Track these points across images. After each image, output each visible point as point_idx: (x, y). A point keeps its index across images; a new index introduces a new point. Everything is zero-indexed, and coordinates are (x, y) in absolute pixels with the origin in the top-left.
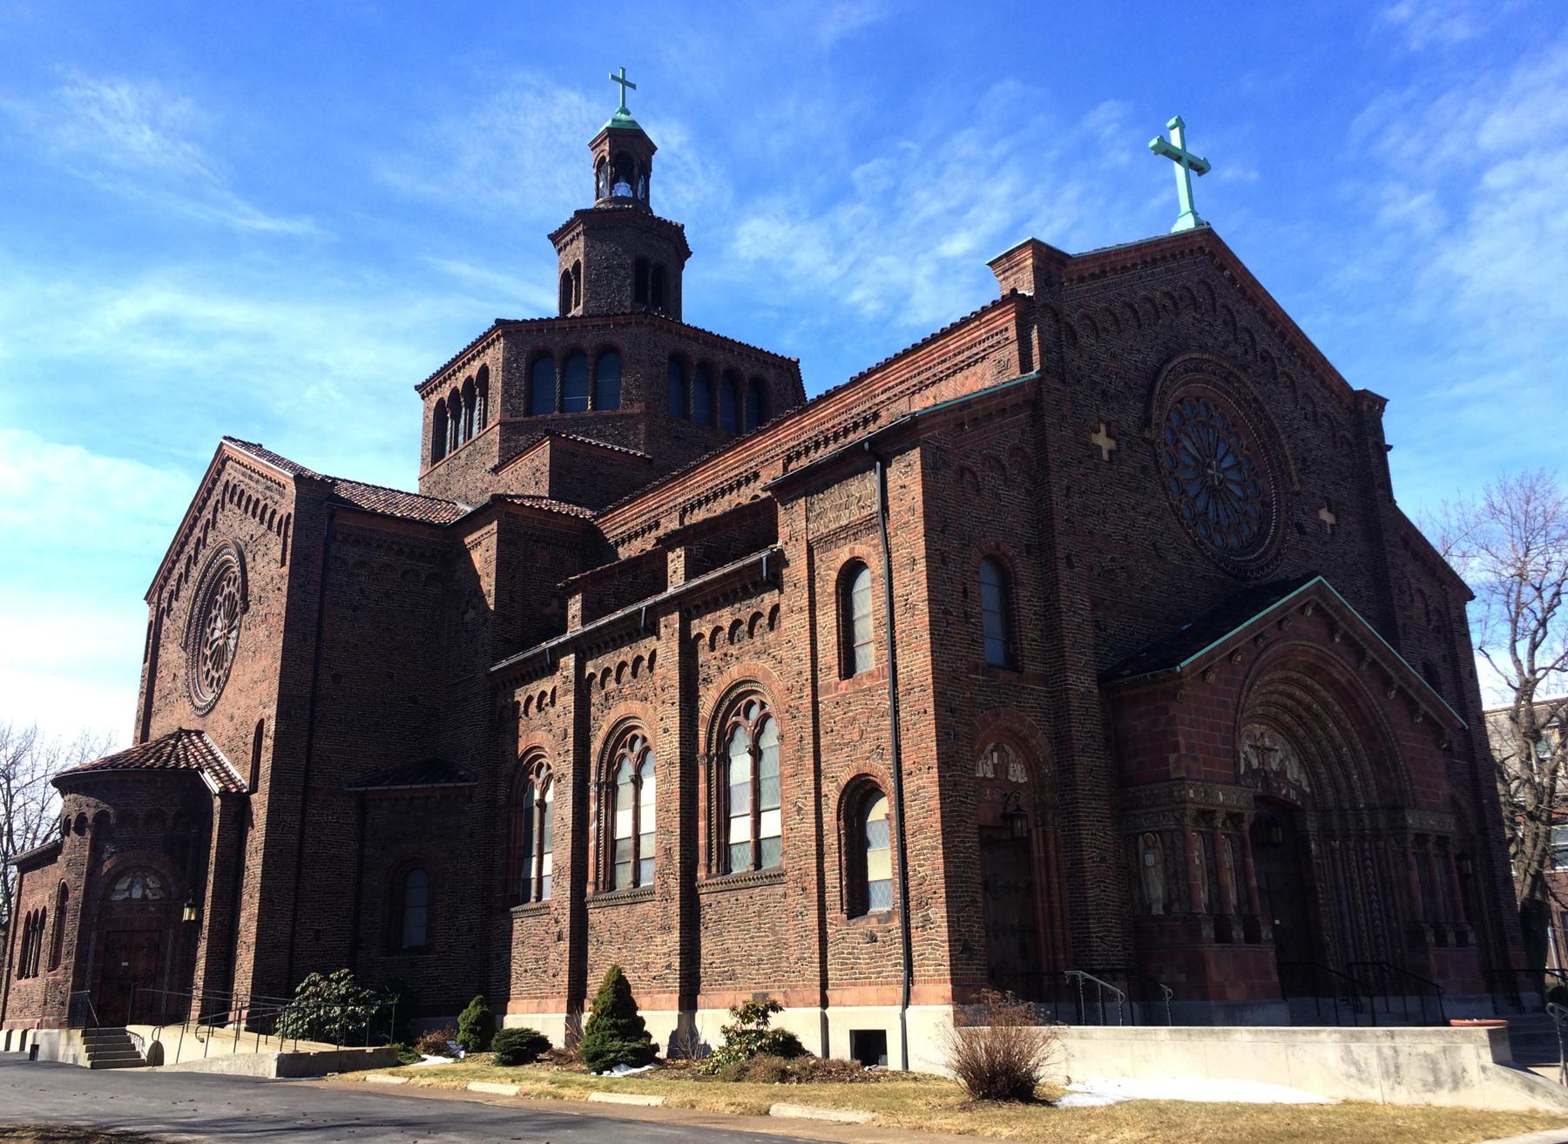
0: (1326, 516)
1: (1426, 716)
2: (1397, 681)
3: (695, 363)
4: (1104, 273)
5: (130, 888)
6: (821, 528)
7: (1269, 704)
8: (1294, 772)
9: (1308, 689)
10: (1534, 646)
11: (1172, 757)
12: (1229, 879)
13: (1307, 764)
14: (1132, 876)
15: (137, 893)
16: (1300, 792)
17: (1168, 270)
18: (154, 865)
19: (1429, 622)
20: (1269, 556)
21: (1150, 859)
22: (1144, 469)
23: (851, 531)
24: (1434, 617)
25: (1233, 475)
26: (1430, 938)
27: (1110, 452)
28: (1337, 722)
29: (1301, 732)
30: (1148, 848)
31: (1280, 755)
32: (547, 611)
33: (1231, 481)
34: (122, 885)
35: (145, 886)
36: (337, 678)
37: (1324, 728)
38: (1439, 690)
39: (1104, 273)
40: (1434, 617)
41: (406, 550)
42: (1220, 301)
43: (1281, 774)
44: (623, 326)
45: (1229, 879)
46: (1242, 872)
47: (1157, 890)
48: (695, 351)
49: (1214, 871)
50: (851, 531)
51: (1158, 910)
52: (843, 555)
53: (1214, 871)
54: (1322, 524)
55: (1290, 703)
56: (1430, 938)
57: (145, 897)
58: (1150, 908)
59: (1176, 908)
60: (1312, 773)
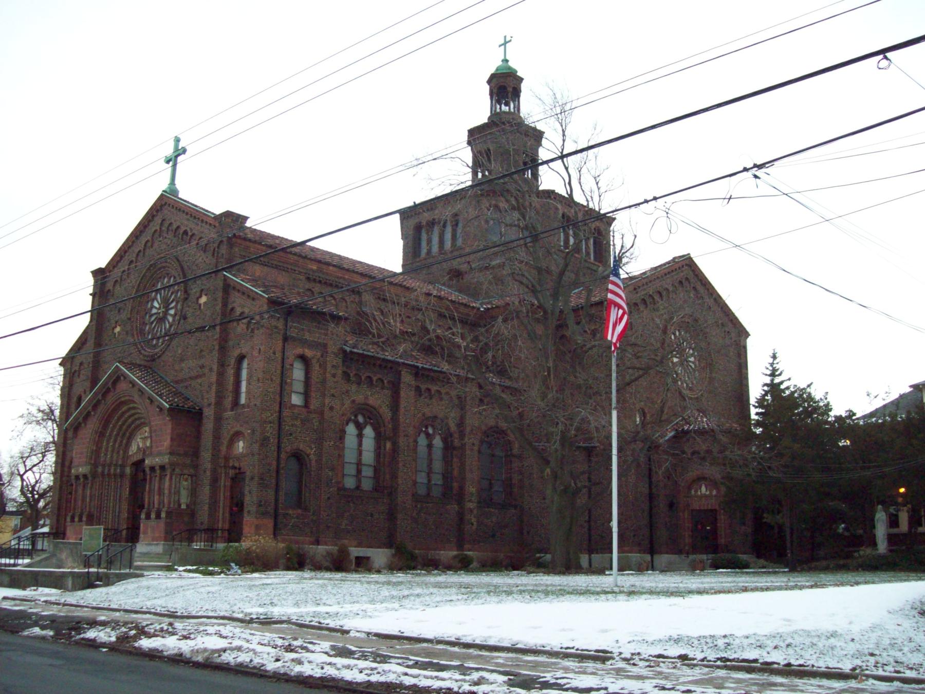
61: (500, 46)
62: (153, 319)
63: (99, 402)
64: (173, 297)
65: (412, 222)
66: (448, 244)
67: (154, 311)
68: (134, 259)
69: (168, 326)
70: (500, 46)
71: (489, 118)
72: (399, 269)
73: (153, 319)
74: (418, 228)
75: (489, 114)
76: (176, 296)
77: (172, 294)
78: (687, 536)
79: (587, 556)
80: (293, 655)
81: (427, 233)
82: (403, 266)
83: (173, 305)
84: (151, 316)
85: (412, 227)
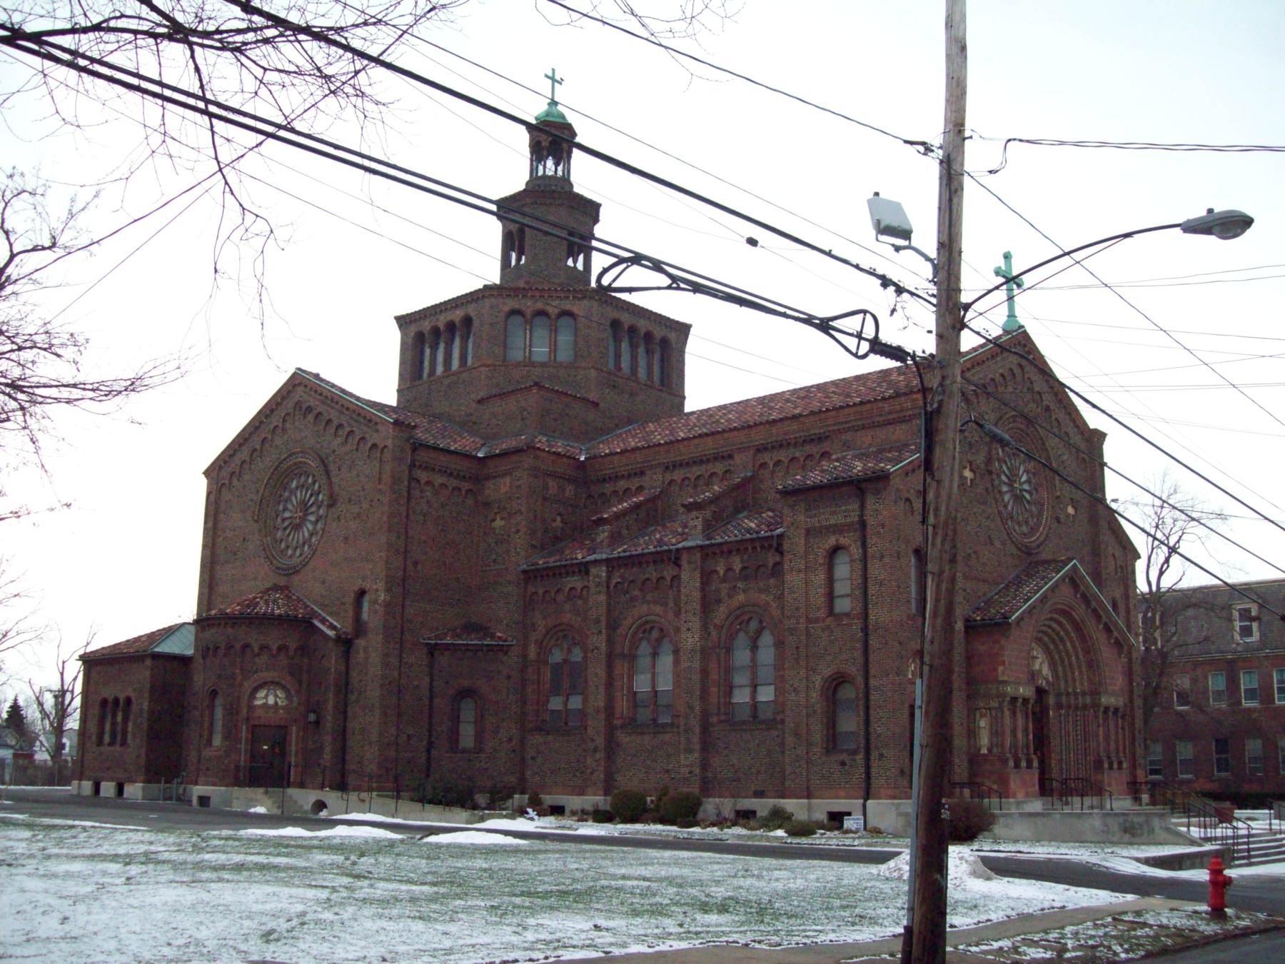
0: (1070, 510)
1: (1116, 639)
2: (1104, 619)
3: (626, 327)
4: (973, 366)
5: (266, 696)
6: (814, 522)
7: (1039, 632)
8: (1046, 671)
9: (1060, 624)
10: (1161, 573)
11: (1001, 669)
12: (1020, 735)
13: (1053, 665)
14: (972, 733)
15: (271, 700)
16: (1048, 682)
17: (1002, 359)
18: (283, 682)
19: (1116, 574)
20: (1042, 539)
21: (983, 723)
22: (987, 489)
23: (838, 529)
24: (1119, 570)
25: (1026, 487)
26: (1106, 766)
27: (971, 480)
28: (1072, 642)
29: (1052, 647)
30: (982, 716)
31: (1040, 660)
32: (554, 525)
33: (1025, 490)
34: (261, 694)
35: (276, 696)
36: (416, 563)
37: (1064, 645)
38: (1118, 615)
39: (973, 366)
40: (1119, 570)
41: (455, 474)
42: (1027, 376)
43: (1040, 671)
44: (579, 299)
45: (1020, 735)
46: (1026, 730)
47: (984, 741)
48: (626, 319)
49: (1014, 731)
50: (838, 529)
51: (984, 751)
52: (832, 541)
53: (1014, 731)
54: (1068, 516)
55: (1049, 631)
56: (1106, 766)
57: (276, 703)
58: (980, 749)
59: (995, 750)
60: (1056, 675)
61: (553, 70)
62: (287, 523)
63: (1098, 617)
64: (313, 499)
65: (413, 329)
66: (455, 364)
67: (287, 515)
68: (258, 447)
69: (306, 534)
70: (553, 70)
71: (527, 184)
72: (391, 399)
73: (287, 523)
74: (420, 337)
75: (527, 178)
76: (316, 499)
77: (311, 495)
78: (243, 742)
79: (661, 688)
80: (171, 926)
81: (431, 347)
82: (400, 391)
83: (313, 509)
84: (284, 520)
85: (412, 334)
